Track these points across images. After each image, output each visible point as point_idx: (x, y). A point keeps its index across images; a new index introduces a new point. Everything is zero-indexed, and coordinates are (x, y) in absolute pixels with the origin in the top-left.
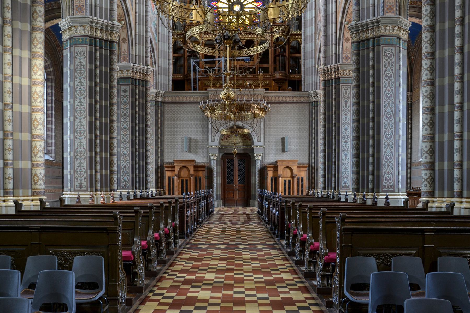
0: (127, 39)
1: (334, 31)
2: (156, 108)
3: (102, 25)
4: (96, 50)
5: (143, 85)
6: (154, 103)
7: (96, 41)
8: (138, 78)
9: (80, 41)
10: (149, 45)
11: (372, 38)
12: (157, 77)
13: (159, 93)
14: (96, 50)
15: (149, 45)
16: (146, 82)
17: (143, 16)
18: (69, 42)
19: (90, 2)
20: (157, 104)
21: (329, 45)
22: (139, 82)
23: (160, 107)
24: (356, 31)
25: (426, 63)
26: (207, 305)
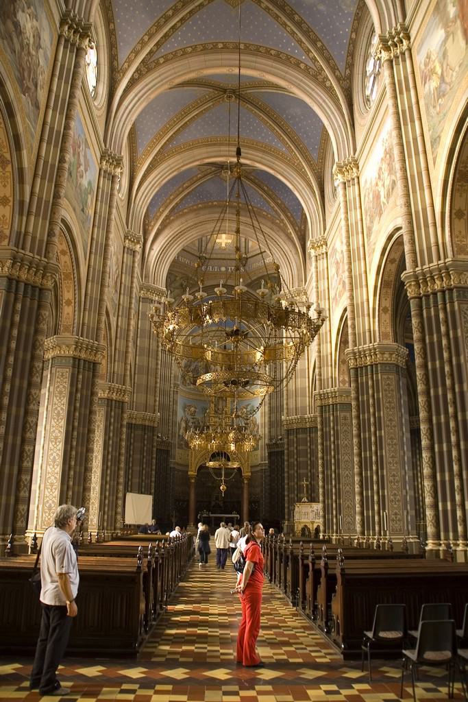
0: (11, 199)
1: (365, 297)
2: (73, 370)
3: (117, 389)
4: (16, 300)
5: (89, 368)
6: (106, 402)
7: (19, 286)
8: (114, 398)
9: (64, 361)
10: (104, 318)
11: (439, 291)
12: (25, 218)
13: (82, 344)
14: (16, 300)
15: (104, 318)
16: (95, 364)
17: (99, 271)
18: (50, 361)
19: (18, 228)
20: (77, 363)
21: (358, 317)
22: (84, 364)
23: (21, 296)
24: (415, 281)
25: (421, 400)
26: (138, 690)
